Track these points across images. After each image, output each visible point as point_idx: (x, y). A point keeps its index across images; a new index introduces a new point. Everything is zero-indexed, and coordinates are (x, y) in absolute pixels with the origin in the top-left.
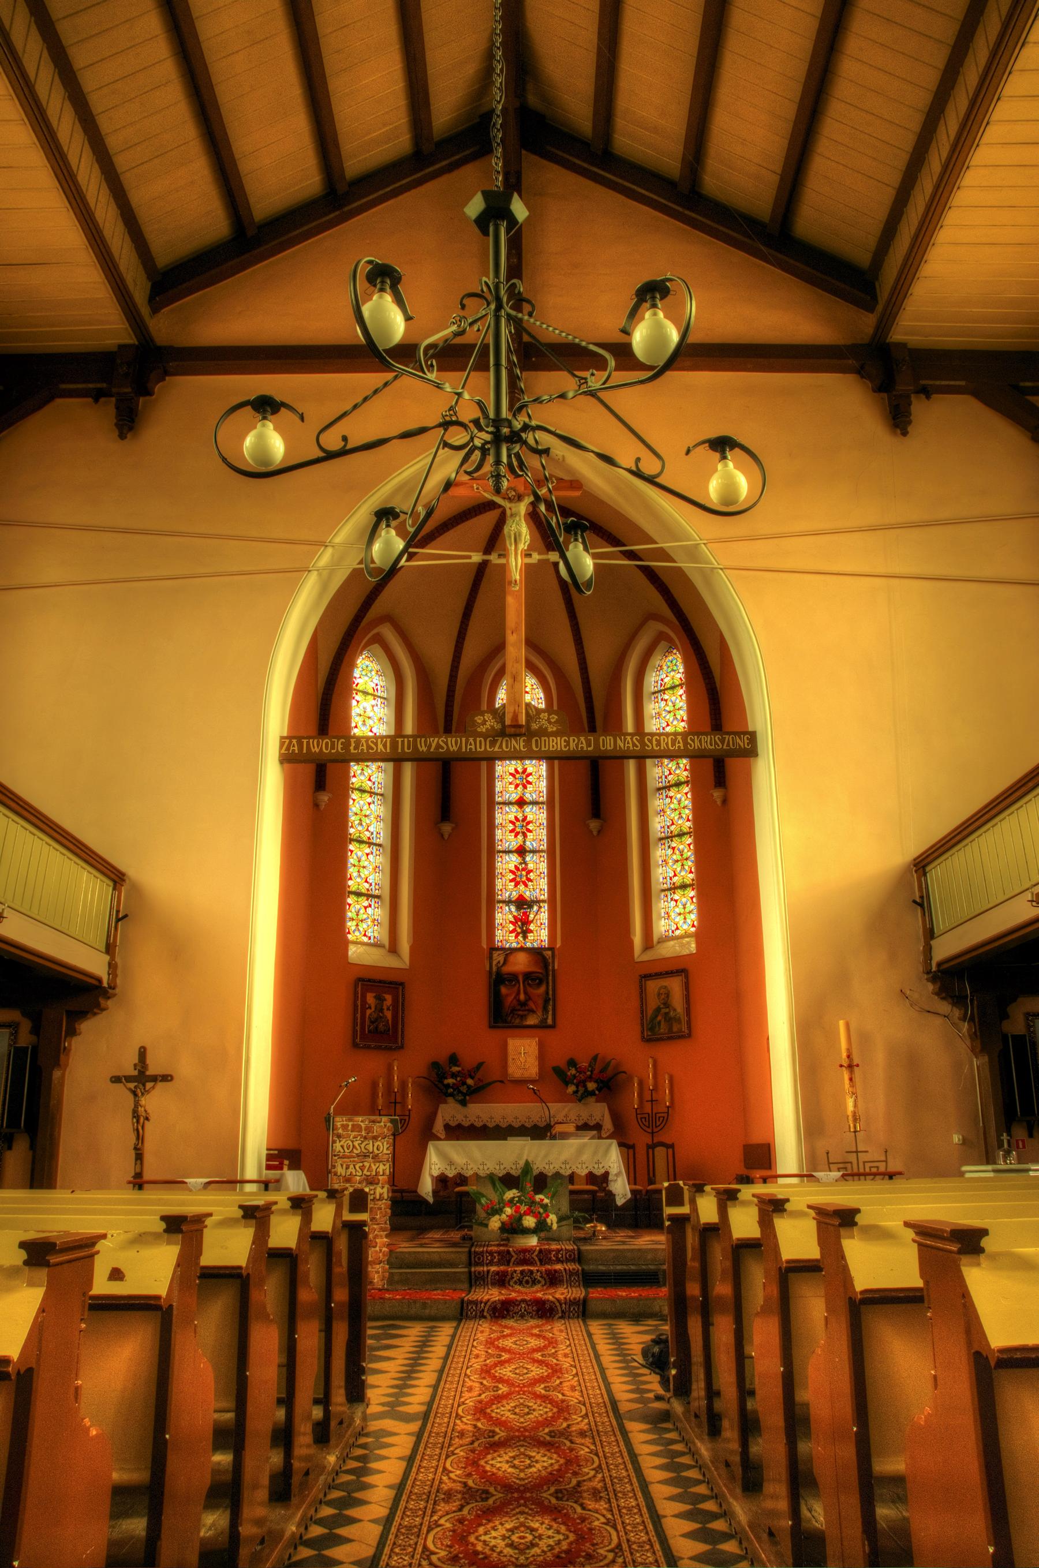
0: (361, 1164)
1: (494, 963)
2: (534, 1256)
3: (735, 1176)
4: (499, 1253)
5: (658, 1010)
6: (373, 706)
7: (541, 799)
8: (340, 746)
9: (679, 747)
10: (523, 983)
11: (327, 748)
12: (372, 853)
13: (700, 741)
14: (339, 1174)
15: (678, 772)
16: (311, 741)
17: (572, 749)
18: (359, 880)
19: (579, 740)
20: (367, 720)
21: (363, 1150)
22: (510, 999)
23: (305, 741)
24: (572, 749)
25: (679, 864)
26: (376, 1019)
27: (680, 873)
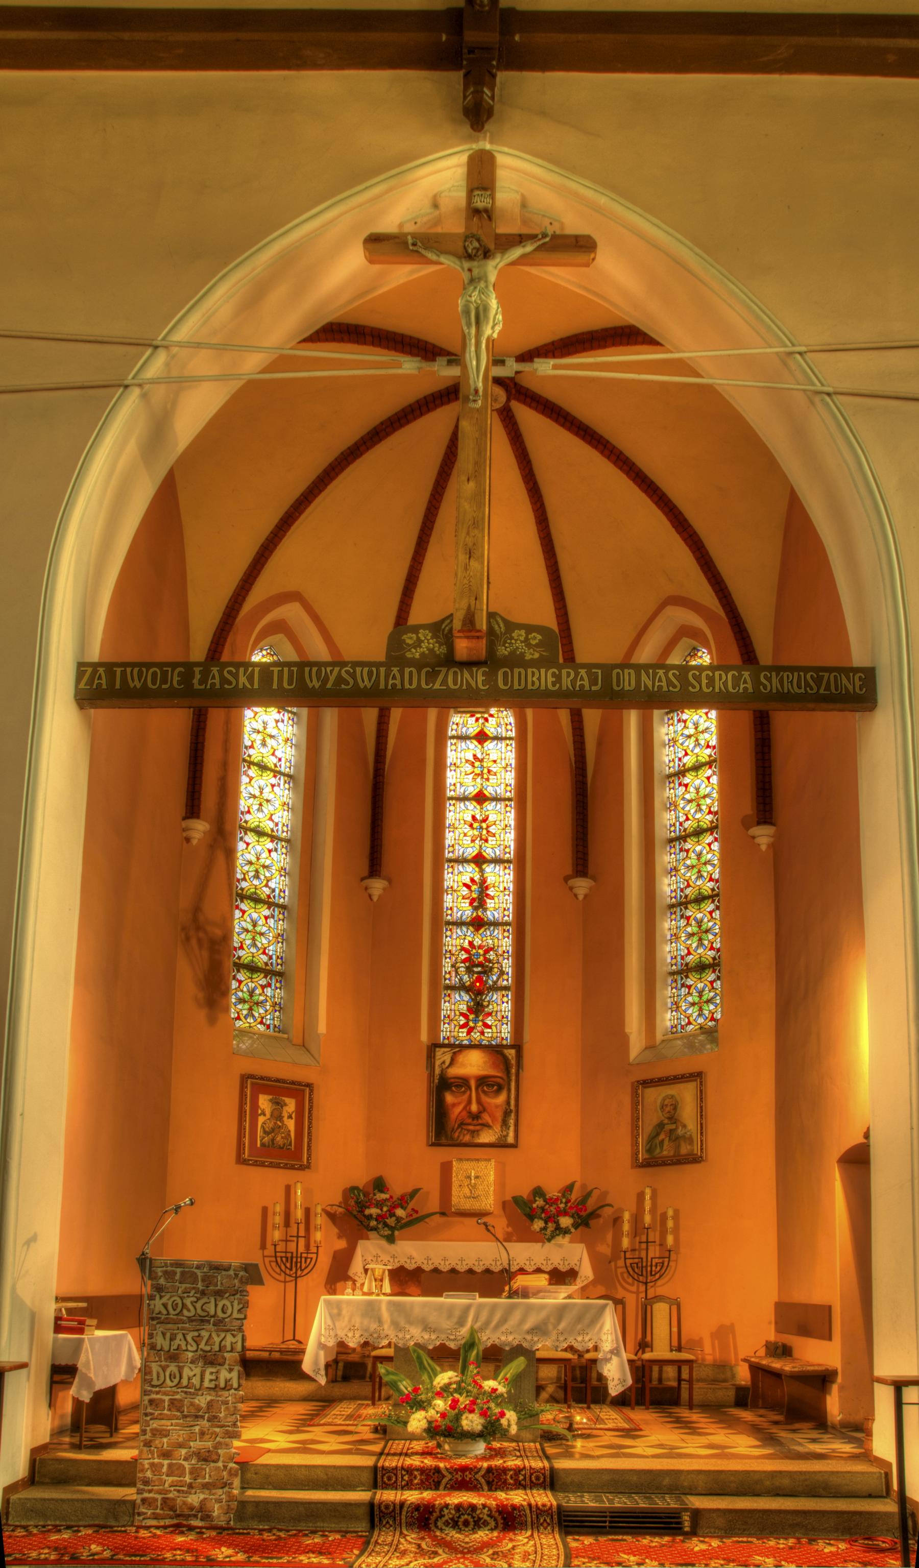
0: (196, 1334)
1: (438, 1063)
2: (479, 1476)
3: (764, 1343)
4: (422, 1470)
5: (661, 1126)
6: (277, 721)
7: (507, 855)
8: (176, 679)
9: (745, 689)
10: (477, 1089)
11: (154, 683)
12: (273, 917)
13: (781, 682)
14: (159, 1347)
15: (698, 816)
16: (129, 670)
17: (564, 688)
18: (253, 950)
19: (577, 674)
20: (268, 740)
21: (199, 1311)
22: (458, 1110)
23: (119, 670)
24: (564, 688)
25: (696, 938)
26: (273, 1130)
27: (695, 951)
